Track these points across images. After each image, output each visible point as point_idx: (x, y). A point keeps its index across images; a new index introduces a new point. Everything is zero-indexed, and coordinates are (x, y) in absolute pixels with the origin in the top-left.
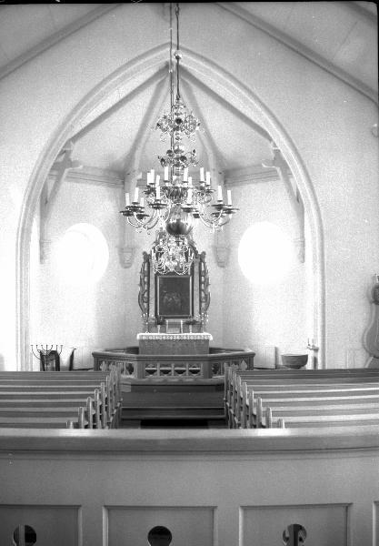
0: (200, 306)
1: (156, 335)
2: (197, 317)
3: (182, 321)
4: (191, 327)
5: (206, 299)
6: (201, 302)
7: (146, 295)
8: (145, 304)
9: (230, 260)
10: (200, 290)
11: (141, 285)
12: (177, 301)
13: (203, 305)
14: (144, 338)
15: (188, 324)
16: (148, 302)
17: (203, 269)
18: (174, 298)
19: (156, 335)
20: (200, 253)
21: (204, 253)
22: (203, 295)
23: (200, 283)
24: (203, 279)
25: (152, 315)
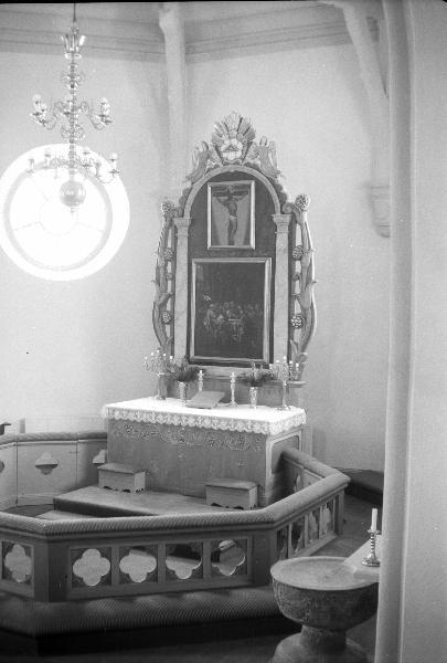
0: (290, 336)
1: (174, 408)
2: (280, 364)
3: (233, 374)
4: (253, 391)
5: (302, 322)
6: (291, 327)
7: (169, 307)
8: (168, 328)
9: (183, 49)
10: (291, 296)
11: (158, 281)
12: (235, 322)
13: (298, 333)
14: (117, 416)
15: (246, 382)
16: (172, 322)
17: (298, 242)
18: (224, 316)
19: (174, 408)
20: (291, 199)
21: (301, 200)
22: (297, 309)
23: (291, 277)
24: (298, 266)
25: (180, 350)
